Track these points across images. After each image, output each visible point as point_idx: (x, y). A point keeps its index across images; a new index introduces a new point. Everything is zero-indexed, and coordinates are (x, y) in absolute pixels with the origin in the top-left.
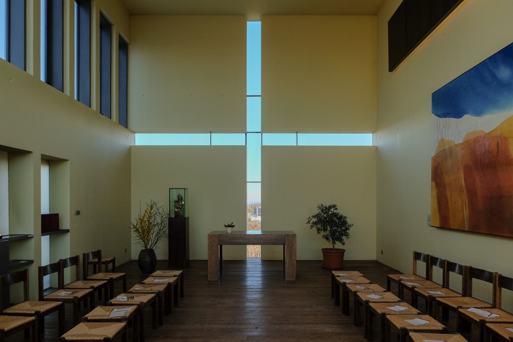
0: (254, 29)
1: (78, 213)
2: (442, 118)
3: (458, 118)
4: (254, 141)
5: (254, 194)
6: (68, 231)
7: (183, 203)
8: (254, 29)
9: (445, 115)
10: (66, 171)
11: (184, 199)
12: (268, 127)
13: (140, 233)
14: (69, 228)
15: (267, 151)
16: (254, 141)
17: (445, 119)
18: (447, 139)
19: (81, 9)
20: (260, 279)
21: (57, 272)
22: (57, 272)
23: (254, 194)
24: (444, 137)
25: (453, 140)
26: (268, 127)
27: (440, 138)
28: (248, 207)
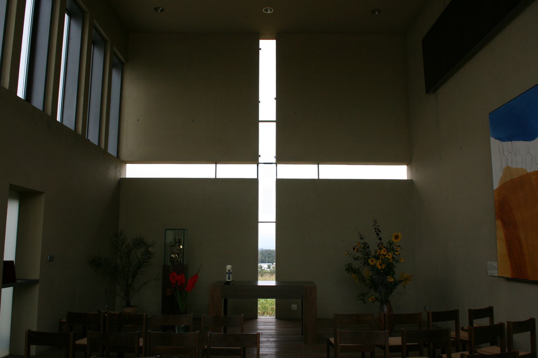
0: (268, 49)
1: (52, 259)
2: (506, 142)
3: (530, 140)
4: (268, 172)
5: (267, 237)
6: (36, 282)
7: (181, 247)
8: (268, 49)
9: (510, 138)
10: (40, 206)
11: (182, 241)
12: (283, 157)
13: (361, 251)
14: (38, 278)
15: (283, 185)
16: (268, 172)
17: (509, 143)
18: (514, 166)
19: (72, 22)
20: (273, 345)
21: (529, 333)
22: (529, 333)
23: (267, 237)
24: (510, 165)
25: (524, 167)
26: (283, 157)
27: (504, 166)
28: (259, 253)
